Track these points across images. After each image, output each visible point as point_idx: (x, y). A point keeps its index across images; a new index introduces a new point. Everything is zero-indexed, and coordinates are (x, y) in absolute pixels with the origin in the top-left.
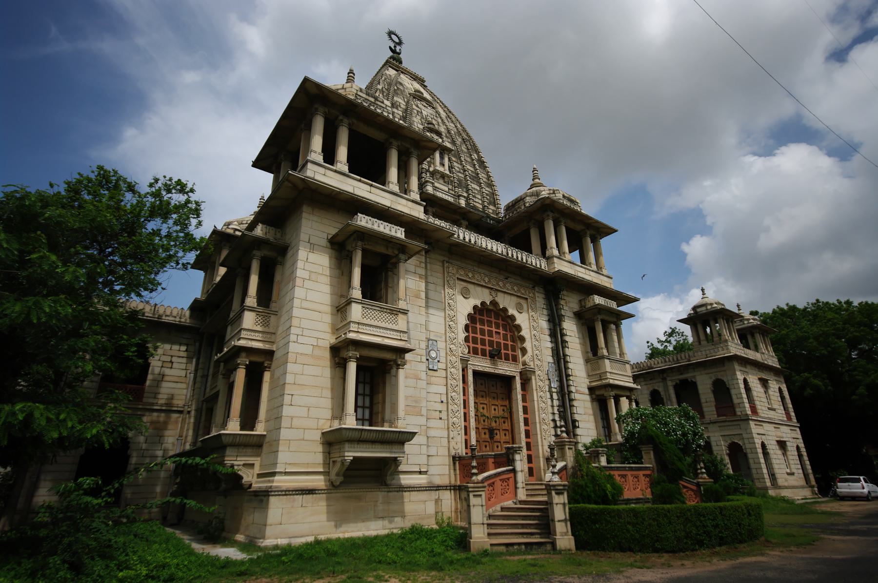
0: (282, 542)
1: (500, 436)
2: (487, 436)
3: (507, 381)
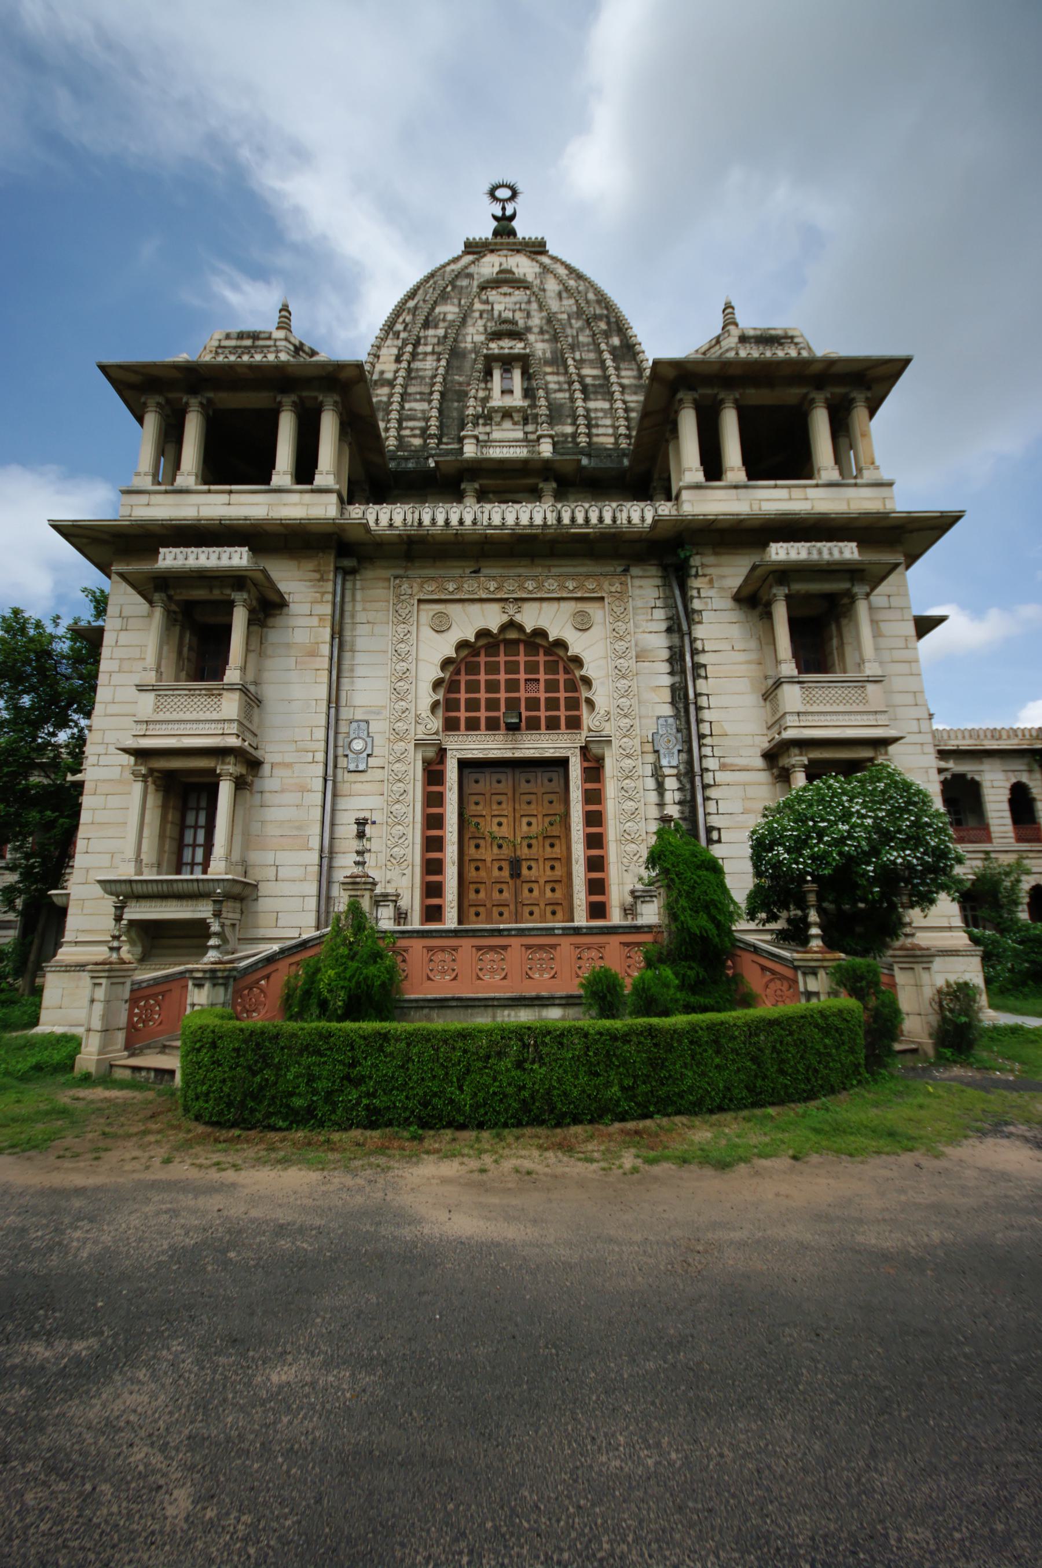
0: (59, 1030)
1: (538, 872)
2: (506, 873)
3: (563, 763)
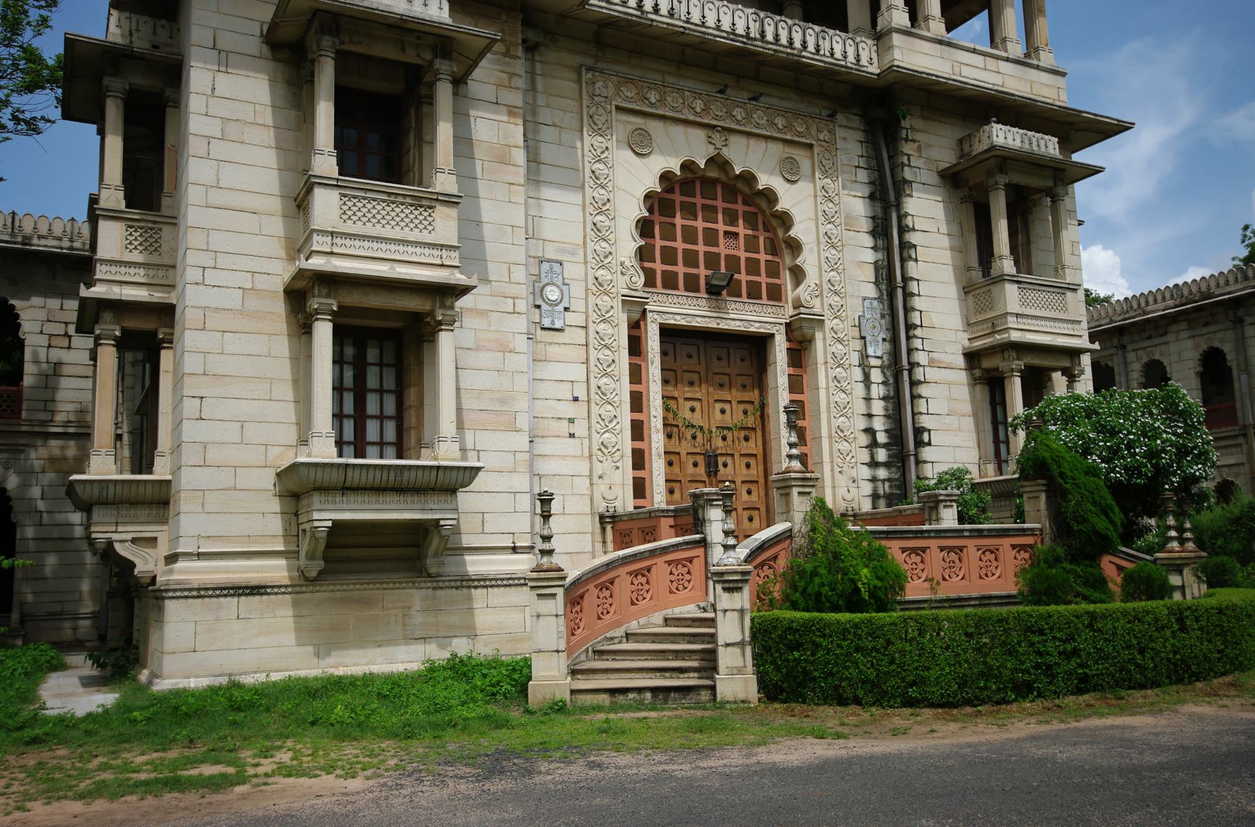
2: (701, 470)
3: (758, 344)
